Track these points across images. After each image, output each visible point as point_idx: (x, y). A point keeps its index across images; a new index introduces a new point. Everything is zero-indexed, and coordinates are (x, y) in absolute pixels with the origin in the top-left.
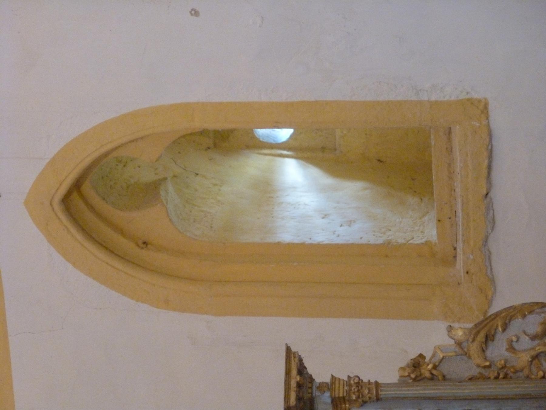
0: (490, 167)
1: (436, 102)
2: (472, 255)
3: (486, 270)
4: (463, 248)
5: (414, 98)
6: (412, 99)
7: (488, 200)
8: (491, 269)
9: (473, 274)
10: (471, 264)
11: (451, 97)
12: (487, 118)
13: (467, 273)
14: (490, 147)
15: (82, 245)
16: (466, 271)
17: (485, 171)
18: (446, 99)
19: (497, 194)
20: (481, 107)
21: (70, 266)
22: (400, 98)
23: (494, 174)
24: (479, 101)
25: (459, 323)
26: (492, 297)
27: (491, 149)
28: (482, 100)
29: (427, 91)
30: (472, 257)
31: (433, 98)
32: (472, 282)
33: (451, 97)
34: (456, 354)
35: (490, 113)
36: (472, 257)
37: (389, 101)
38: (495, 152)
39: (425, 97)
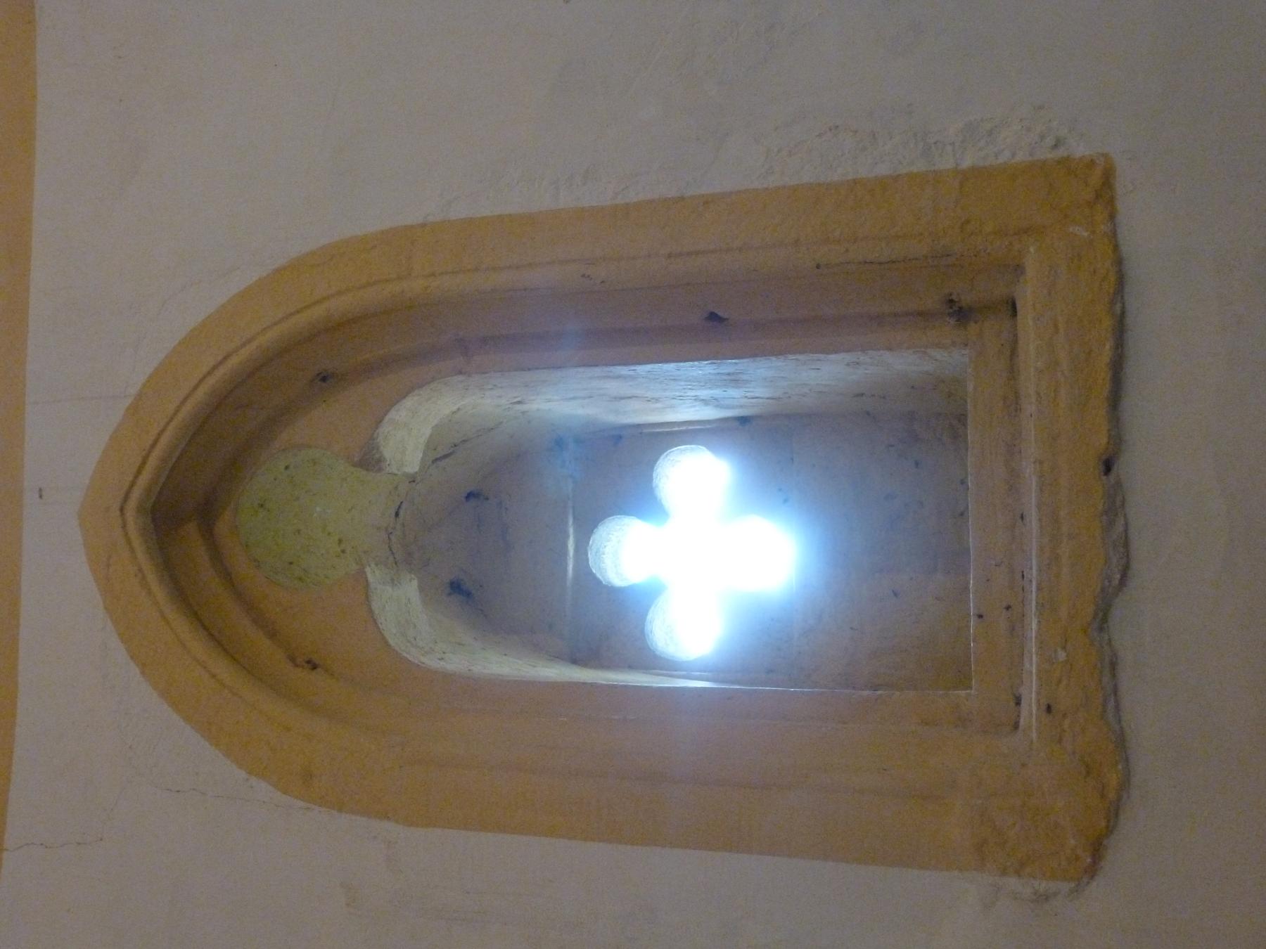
0: (1117, 366)
1: (977, 173)
2: (1064, 648)
3: (1104, 705)
4: (1039, 629)
5: (920, 166)
6: (915, 169)
7: (1112, 477)
8: (1117, 708)
9: (1065, 715)
10: (1060, 681)
11: (1014, 155)
12: (1112, 217)
13: (1049, 709)
14: (1118, 307)
15: (163, 616)
16: (1044, 708)
17: (1103, 375)
18: (1001, 160)
19: (1134, 466)
20: (1095, 179)
21: (135, 670)
22: (883, 170)
23: (1132, 401)
24: (1092, 163)
25: (1019, 876)
26: (1119, 799)
27: (1123, 313)
28: (1097, 161)
29: (953, 144)
30: (1062, 655)
31: (967, 163)
32: (1060, 741)
33: (1014, 155)
34: (1112, 695)
35: (1120, 206)
36: (1062, 655)
37: (855, 182)
38: (1129, 320)
39: (945, 163)
